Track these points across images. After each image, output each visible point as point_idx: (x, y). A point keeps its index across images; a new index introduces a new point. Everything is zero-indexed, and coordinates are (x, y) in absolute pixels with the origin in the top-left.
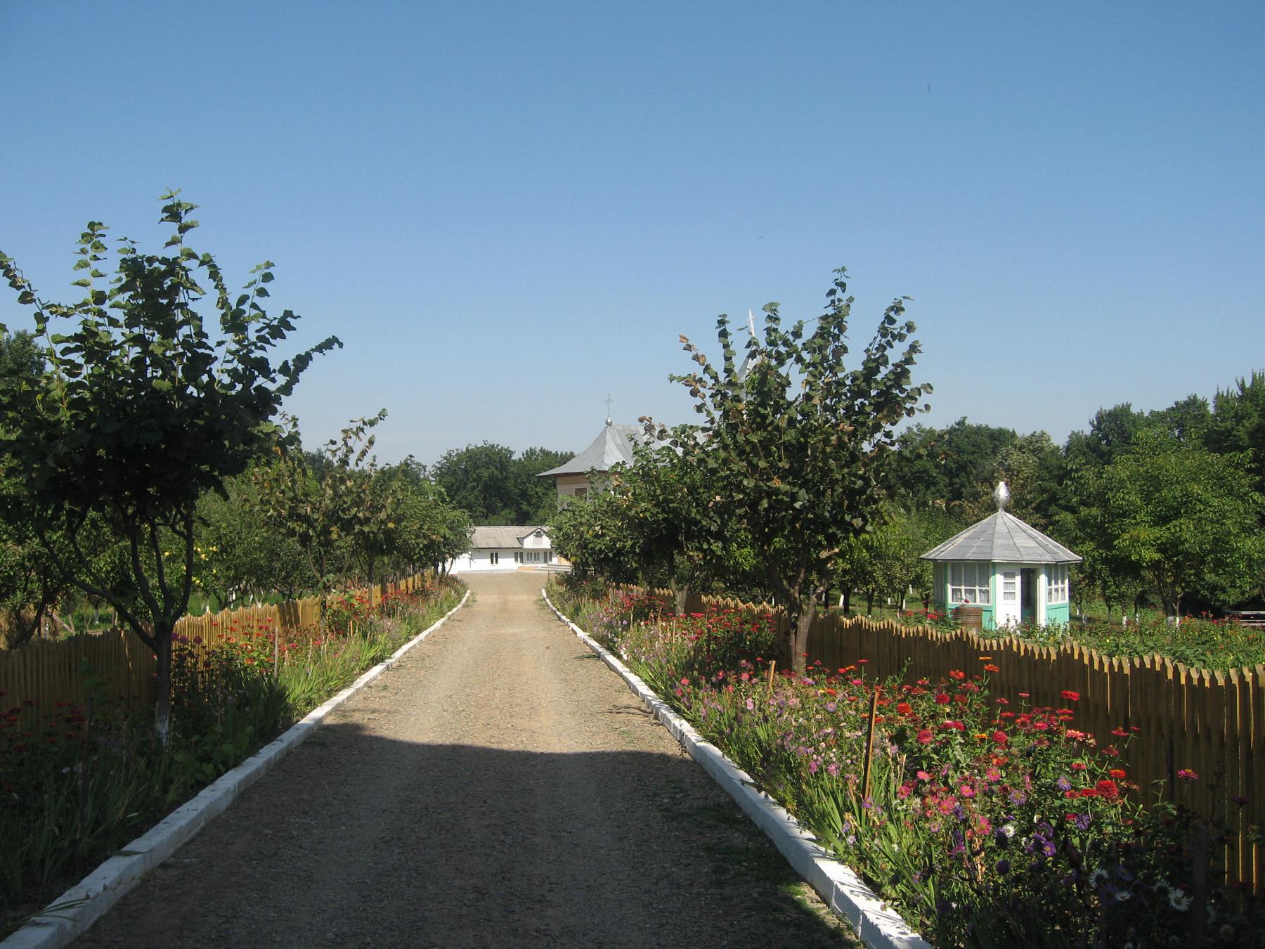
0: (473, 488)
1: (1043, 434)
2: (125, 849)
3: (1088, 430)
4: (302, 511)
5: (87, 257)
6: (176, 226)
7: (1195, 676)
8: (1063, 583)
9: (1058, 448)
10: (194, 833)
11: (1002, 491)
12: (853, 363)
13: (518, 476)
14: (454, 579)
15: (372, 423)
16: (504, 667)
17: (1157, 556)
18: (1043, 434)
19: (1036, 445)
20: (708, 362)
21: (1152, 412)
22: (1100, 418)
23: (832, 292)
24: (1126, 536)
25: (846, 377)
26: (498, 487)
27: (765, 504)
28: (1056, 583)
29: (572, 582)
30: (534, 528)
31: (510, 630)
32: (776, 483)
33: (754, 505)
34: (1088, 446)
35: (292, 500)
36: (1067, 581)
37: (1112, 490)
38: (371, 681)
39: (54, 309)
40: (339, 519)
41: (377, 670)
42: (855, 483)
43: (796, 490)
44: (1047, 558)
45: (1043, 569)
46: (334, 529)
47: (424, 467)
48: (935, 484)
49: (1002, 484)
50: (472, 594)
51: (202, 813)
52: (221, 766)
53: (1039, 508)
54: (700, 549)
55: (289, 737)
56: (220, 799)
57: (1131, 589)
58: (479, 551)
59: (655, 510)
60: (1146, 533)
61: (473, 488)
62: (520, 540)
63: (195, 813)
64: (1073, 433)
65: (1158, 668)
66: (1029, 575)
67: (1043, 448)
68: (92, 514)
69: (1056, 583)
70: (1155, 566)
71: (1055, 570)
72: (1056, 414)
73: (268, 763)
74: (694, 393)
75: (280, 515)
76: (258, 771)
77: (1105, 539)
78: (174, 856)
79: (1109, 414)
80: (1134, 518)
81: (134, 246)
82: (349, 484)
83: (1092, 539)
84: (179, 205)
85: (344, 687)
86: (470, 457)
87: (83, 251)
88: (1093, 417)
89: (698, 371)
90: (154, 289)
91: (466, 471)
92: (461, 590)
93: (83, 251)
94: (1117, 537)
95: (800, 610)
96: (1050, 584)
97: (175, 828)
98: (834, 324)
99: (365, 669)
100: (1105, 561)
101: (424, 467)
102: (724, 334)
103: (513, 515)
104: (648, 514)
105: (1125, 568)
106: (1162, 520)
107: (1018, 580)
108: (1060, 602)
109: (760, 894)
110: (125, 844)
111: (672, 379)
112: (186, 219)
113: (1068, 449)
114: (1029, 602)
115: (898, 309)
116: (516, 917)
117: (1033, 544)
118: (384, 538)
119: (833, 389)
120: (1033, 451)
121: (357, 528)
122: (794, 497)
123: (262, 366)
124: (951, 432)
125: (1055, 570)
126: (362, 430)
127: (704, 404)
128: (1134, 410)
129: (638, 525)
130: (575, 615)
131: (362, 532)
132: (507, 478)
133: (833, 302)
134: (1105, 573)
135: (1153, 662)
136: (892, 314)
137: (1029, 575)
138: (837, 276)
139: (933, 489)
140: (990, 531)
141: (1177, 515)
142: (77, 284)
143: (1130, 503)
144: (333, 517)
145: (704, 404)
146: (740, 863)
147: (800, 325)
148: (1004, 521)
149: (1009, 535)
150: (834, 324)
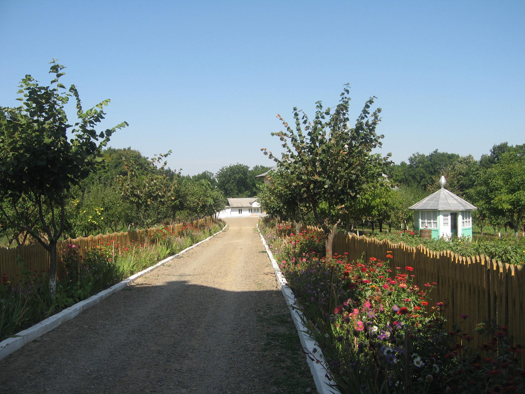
0: (233, 183)
1: (470, 156)
2: (17, 334)
3: (489, 154)
4: (136, 193)
5: (23, 89)
6: (56, 74)
7: (461, 260)
8: (469, 219)
9: (476, 162)
10: (54, 327)
11: (443, 180)
12: (351, 125)
13: (251, 177)
14: (220, 220)
15: (166, 156)
16: (239, 256)
17: (510, 207)
18: (470, 156)
19: (467, 161)
20: (289, 126)
21: (517, 146)
22: (494, 148)
23: (343, 94)
24: (496, 199)
25: (349, 131)
26: (239, 182)
27: (312, 186)
28: (466, 219)
29: (266, 221)
30: (257, 199)
31: (237, 241)
32: (316, 177)
33: (308, 187)
34: (489, 160)
35: (132, 188)
36: (471, 218)
37: (490, 179)
38: (165, 263)
39: (6, 109)
40: (152, 196)
41: (171, 257)
42: (352, 176)
43: (324, 180)
44: (462, 208)
45: (460, 213)
46: (149, 200)
47: (213, 174)
48: (425, 178)
49: (443, 177)
50: (228, 226)
51: (59, 319)
52: (77, 299)
53: (460, 187)
54: (305, 206)
55: (117, 286)
56: (71, 313)
57: (503, 221)
58: (234, 208)
59: (286, 190)
60: (504, 197)
61: (233, 183)
62: (251, 204)
63: (56, 319)
64: (483, 155)
65: (448, 256)
66: (454, 215)
67: (470, 162)
68: (23, 196)
69: (466, 219)
70: (510, 211)
71: (466, 213)
72: (473, 145)
73: (101, 298)
74: (282, 139)
75: (127, 194)
76: (95, 301)
77: (488, 200)
78: (41, 337)
79: (499, 147)
80: (500, 191)
81: (37, 83)
82: (155, 181)
83: (482, 199)
84: (58, 66)
85: (151, 266)
86: (231, 170)
87: (22, 86)
88: (491, 148)
89: (285, 131)
90: (41, 99)
91: (230, 176)
92: (222, 224)
93: (22, 86)
94: (493, 199)
95: (329, 232)
96: (463, 219)
97: (43, 325)
98: (343, 108)
99: (164, 258)
100: (488, 209)
101: (213, 174)
102: (296, 115)
103: (249, 194)
104: (283, 192)
105: (497, 212)
106: (512, 191)
107: (449, 217)
108: (468, 227)
109: (279, 354)
110: (18, 332)
111: (273, 134)
112: (60, 72)
113: (481, 162)
114: (454, 227)
115: (371, 102)
116: (170, 364)
117: (456, 202)
118: (186, 205)
119: (342, 138)
120: (466, 163)
121: (159, 199)
122: (324, 183)
123: (93, 133)
124: (431, 156)
125: (466, 213)
126: (161, 158)
127: (286, 144)
128: (509, 145)
129: (280, 196)
130: (264, 233)
131: (161, 201)
132: (247, 178)
133: (343, 98)
134: (488, 214)
135: (447, 253)
136: (368, 104)
137: (454, 215)
138: (345, 87)
139: (424, 180)
140: (438, 197)
141: (519, 189)
142: (17, 99)
143: (498, 184)
144: (149, 195)
145: (286, 144)
146: (278, 341)
147: (329, 109)
148: (444, 193)
149: (446, 199)
150: (343, 108)
